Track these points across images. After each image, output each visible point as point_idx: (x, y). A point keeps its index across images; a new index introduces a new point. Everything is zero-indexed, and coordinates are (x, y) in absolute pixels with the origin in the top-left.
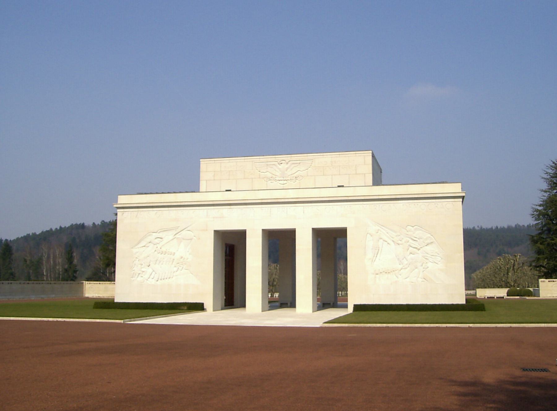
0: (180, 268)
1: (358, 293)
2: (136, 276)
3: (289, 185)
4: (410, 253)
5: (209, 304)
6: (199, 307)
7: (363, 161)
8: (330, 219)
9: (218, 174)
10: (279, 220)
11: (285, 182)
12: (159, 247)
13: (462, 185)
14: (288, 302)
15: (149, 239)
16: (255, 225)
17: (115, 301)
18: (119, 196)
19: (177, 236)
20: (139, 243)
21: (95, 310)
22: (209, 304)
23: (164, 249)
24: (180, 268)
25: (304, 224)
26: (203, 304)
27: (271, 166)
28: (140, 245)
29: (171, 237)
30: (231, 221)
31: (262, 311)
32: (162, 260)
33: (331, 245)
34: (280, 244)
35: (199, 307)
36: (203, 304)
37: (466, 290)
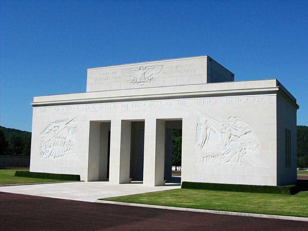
0: (69, 149)
1: (189, 172)
2: (43, 154)
3: (146, 85)
4: (233, 142)
5: (84, 176)
6: (77, 178)
7: (199, 64)
8: (170, 111)
9: (102, 79)
10: (133, 112)
11: (143, 83)
12: (56, 133)
13: (275, 187)
14: (104, 177)
15: (50, 128)
16: (117, 116)
17: (30, 171)
18: (34, 97)
19: (67, 125)
20: (45, 130)
21: (16, 177)
22: (84, 176)
23: (59, 135)
24: (69, 149)
25: (151, 115)
26: (79, 176)
27: (133, 71)
28: (45, 132)
29: (64, 126)
30: (101, 113)
31: (120, 184)
32: (59, 142)
33: (172, 131)
34: (135, 130)
35: (77, 178)
36: (79, 176)
37: (181, 178)
